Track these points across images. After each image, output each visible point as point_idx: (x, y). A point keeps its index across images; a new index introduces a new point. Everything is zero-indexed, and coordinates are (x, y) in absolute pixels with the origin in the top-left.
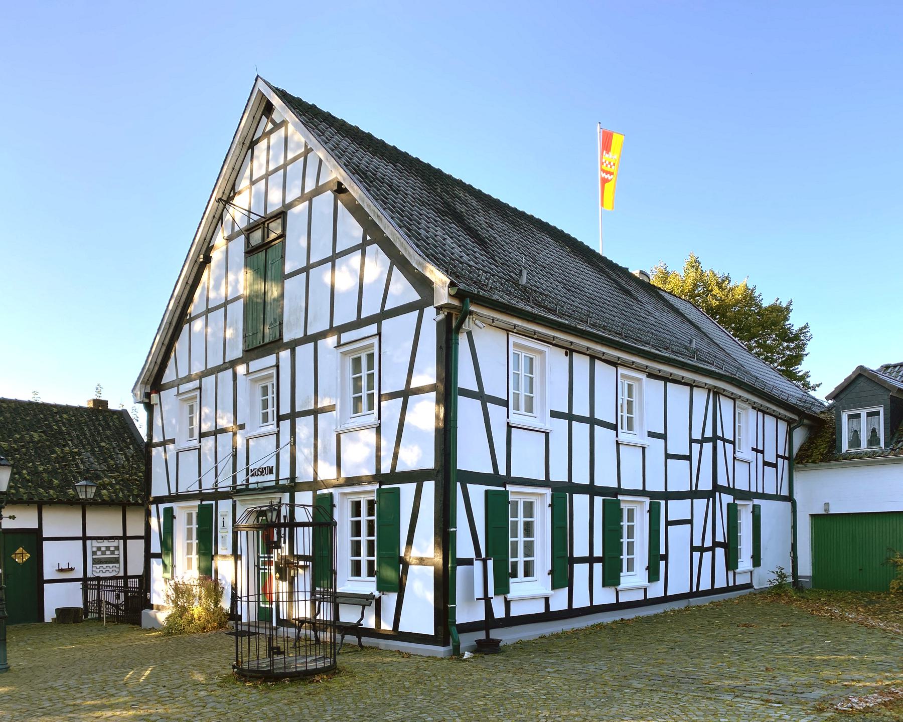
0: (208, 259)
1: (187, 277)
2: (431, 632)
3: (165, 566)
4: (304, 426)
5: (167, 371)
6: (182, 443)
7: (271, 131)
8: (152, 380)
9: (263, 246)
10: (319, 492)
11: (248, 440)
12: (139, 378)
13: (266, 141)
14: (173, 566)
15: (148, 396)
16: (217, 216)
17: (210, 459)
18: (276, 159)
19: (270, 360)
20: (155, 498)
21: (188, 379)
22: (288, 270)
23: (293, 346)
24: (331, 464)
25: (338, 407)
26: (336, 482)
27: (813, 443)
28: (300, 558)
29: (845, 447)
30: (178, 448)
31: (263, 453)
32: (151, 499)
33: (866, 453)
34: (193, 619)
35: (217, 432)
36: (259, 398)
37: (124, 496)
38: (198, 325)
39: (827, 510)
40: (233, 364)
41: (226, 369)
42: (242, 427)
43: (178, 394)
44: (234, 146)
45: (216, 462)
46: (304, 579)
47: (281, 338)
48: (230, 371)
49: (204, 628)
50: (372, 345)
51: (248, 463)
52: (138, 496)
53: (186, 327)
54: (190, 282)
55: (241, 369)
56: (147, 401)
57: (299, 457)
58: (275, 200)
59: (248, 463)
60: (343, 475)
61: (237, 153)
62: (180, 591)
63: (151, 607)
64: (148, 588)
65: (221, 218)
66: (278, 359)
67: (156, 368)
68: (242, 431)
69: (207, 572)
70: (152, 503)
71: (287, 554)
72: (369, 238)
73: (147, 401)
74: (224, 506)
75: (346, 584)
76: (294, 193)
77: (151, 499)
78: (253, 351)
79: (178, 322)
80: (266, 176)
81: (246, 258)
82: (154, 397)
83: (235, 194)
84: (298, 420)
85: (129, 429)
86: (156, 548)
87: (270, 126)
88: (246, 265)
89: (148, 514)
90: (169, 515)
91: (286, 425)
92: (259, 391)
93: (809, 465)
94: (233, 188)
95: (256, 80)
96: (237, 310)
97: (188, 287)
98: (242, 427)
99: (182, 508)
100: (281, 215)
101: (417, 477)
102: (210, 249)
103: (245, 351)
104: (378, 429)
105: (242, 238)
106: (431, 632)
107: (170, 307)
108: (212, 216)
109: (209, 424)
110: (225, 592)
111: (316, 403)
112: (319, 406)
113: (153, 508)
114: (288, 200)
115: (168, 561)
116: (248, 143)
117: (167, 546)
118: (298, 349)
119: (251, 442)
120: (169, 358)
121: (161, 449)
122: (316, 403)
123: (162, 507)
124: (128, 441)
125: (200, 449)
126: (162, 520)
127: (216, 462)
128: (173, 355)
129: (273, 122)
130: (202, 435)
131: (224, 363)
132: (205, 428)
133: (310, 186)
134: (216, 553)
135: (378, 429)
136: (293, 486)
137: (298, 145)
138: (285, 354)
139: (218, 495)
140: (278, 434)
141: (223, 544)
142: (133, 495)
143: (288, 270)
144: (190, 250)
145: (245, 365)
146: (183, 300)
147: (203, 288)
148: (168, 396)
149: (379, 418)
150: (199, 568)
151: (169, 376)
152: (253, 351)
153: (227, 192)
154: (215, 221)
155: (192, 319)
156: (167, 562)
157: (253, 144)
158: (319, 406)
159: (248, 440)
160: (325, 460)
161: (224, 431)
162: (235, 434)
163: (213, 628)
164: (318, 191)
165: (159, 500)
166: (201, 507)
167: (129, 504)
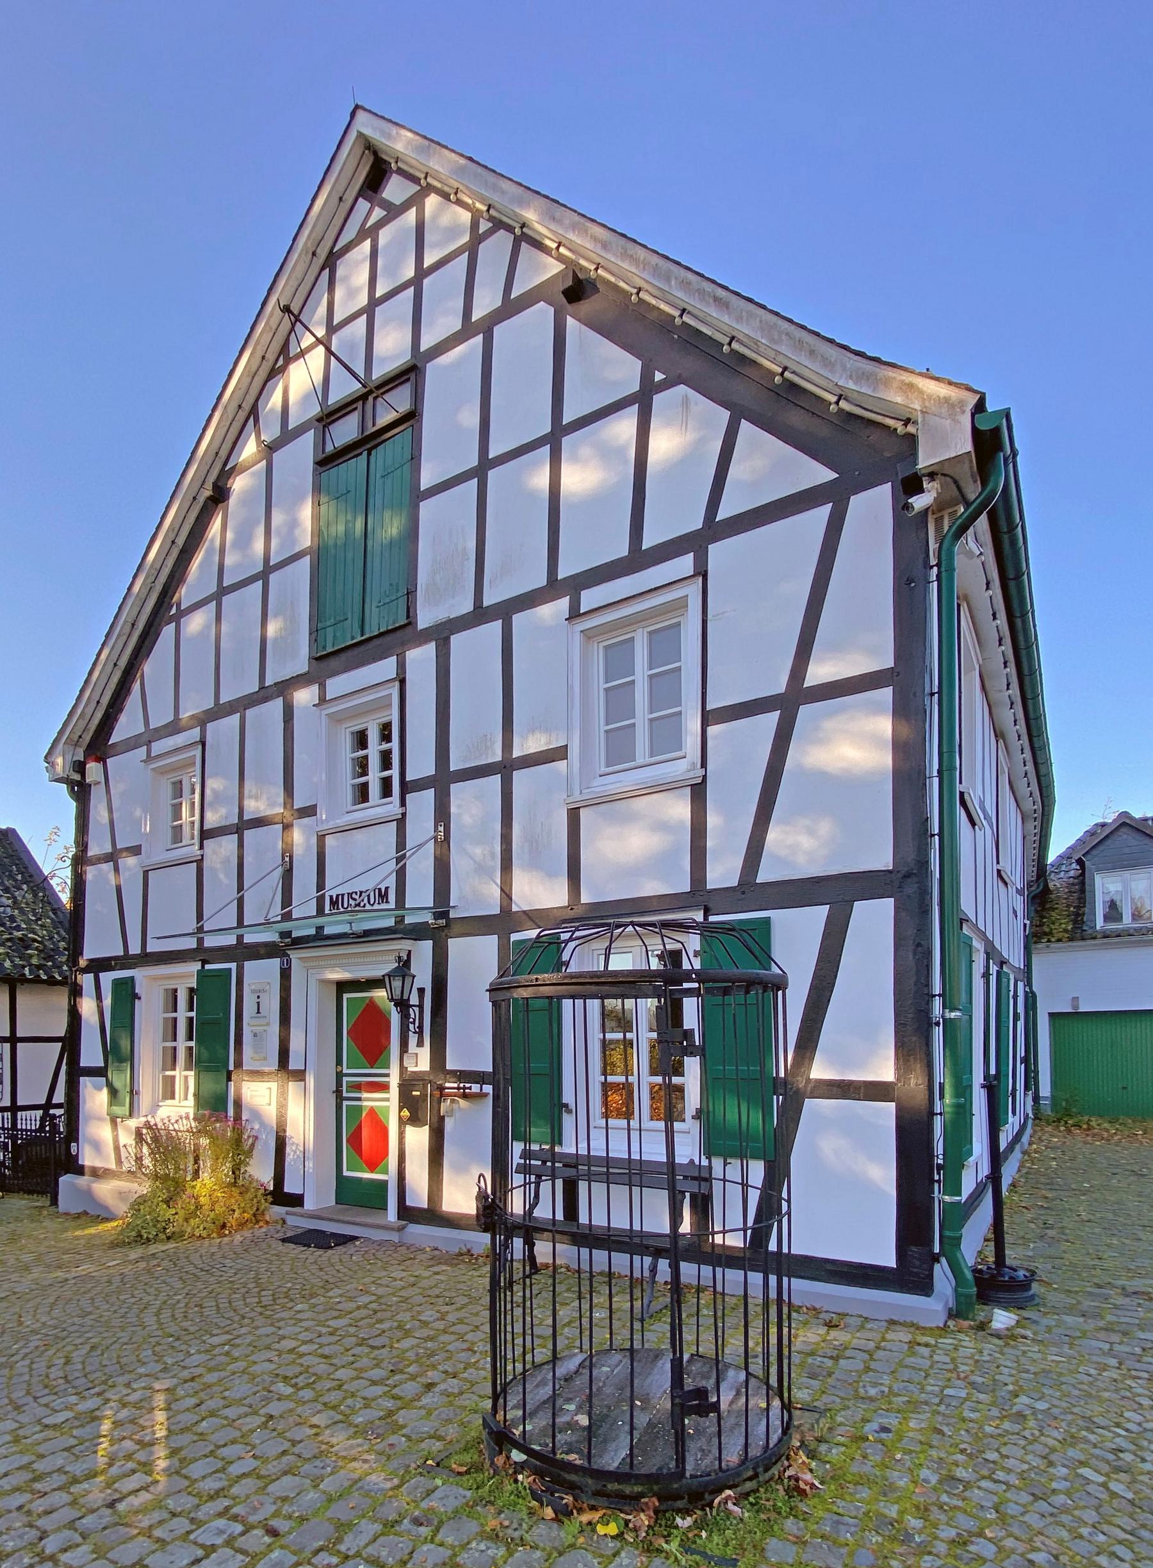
0: (220, 495)
1: (176, 529)
2: (889, 1260)
3: (113, 1093)
4: (473, 804)
5: (123, 719)
6: (157, 853)
7: (381, 224)
8: (87, 738)
9: (365, 437)
10: (514, 937)
11: (321, 839)
12: (61, 733)
13: (367, 245)
14: (133, 1093)
15: (80, 767)
16: (247, 406)
17: (225, 881)
18: (393, 271)
19: (387, 667)
20: (91, 961)
21: (174, 728)
22: (426, 482)
23: (442, 634)
24: (551, 875)
25: (574, 752)
26: (571, 914)
27: (1043, 917)
28: (464, 1076)
29: (1100, 923)
30: (148, 862)
31: (361, 862)
32: (82, 963)
33: (1127, 930)
34: (198, 1207)
35: (242, 826)
36: (347, 754)
37: (15, 966)
38: (196, 623)
39: (1076, 1006)
40: (285, 688)
41: (266, 700)
42: (309, 811)
43: (149, 758)
44: (295, 256)
45: (240, 888)
46: (471, 1121)
47: (411, 622)
48: (279, 702)
49: (224, 1226)
50: (681, 604)
51: (321, 886)
52: (39, 967)
53: (168, 631)
54: (181, 541)
55: (304, 697)
56: (77, 777)
57: (458, 864)
58: (392, 346)
59: (321, 886)
60: (585, 898)
61: (299, 273)
62: (159, 1142)
63: (80, 1170)
64: (73, 1134)
65: (254, 412)
66: (401, 666)
67: (99, 715)
68: (306, 820)
69: (216, 1105)
70: (85, 971)
71: (427, 1068)
72: (659, 376)
73: (77, 777)
74: (261, 975)
75: (587, 1134)
76: (441, 323)
77: (82, 963)
78: (327, 660)
79: (156, 614)
80: (369, 310)
81: (317, 475)
82: (93, 770)
83: (289, 361)
84: (457, 790)
85: (20, 859)
86: (91, 1054)
87: (378, 213)
88: (317, 489)
89: (76, 992)
90: (126, 994)
91: (423, 803)
92: (346, 742)
93: (1053, 945)
94: (285, 348)
95: (353, 115)
96: (297, 581)
97: (175, 553)
98: (309, 811)
99: (156, 979)
100: (410, 374)
101: (838, 893)
102: (227, 472)
103: (318, 659)
104: (699, 792)
105: (310, 436)
106: (889, 1260)
107: (136, 588)
108: (234, 405)
109: (223, 811)
110: (259, 1146)
111: (507, 745)
112: (516, 754)
113: (86, 981)
114: (426, 343)
115: (120, 1080)
116: (323, 254)
117: (119, 1052)
118: (457, 641)
119: (330, 841)
120: (128, 692)
121: (107, 867)
122: (507, 745)
123: (107, 978)
124: (19, 877)
125: (200, 862)
126: (107, 1002)
127: (240, 888)
128: (136, 687)
129: (386, 205)
130: (206, 835)
131: (262, 688)
132: (213, 819)
133: (485, 303)
134: (239, 1064)
135: (699, 792)
136: (442, 927)
137: (453, 231)
138: (422, 657)
139: (244, 952)
140: (401, 822)
141: (257, 1048)
142: (31, 965)
143: (426, 482)
144: (168, 508)
145: (315, 688)
146: (163, 578)
147: (210, 551)
148: (126, 770)
149: (704, 764)
150: (197, 1095)
151: (126, 727)
152: (327, 660)
153: (271, 357)
154: (242, 415)
155: (182, 613)
156: (117, 1084)
157: (331, 262)
158: (516, 754)
159: (321, 839)
160: (535, 864)
161: (260, 822)
162: (287, 827)
163: (242, 1225)
164: (510, 308)
165: (98, 966)
166: (202, 975)
167: (24, 980)
